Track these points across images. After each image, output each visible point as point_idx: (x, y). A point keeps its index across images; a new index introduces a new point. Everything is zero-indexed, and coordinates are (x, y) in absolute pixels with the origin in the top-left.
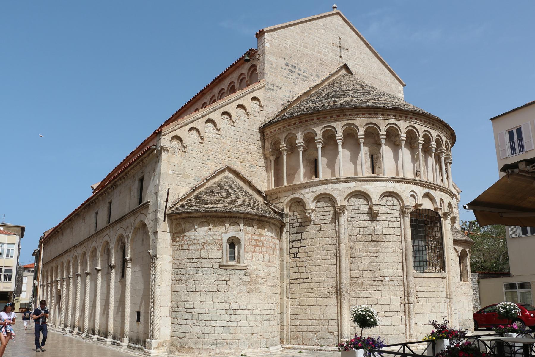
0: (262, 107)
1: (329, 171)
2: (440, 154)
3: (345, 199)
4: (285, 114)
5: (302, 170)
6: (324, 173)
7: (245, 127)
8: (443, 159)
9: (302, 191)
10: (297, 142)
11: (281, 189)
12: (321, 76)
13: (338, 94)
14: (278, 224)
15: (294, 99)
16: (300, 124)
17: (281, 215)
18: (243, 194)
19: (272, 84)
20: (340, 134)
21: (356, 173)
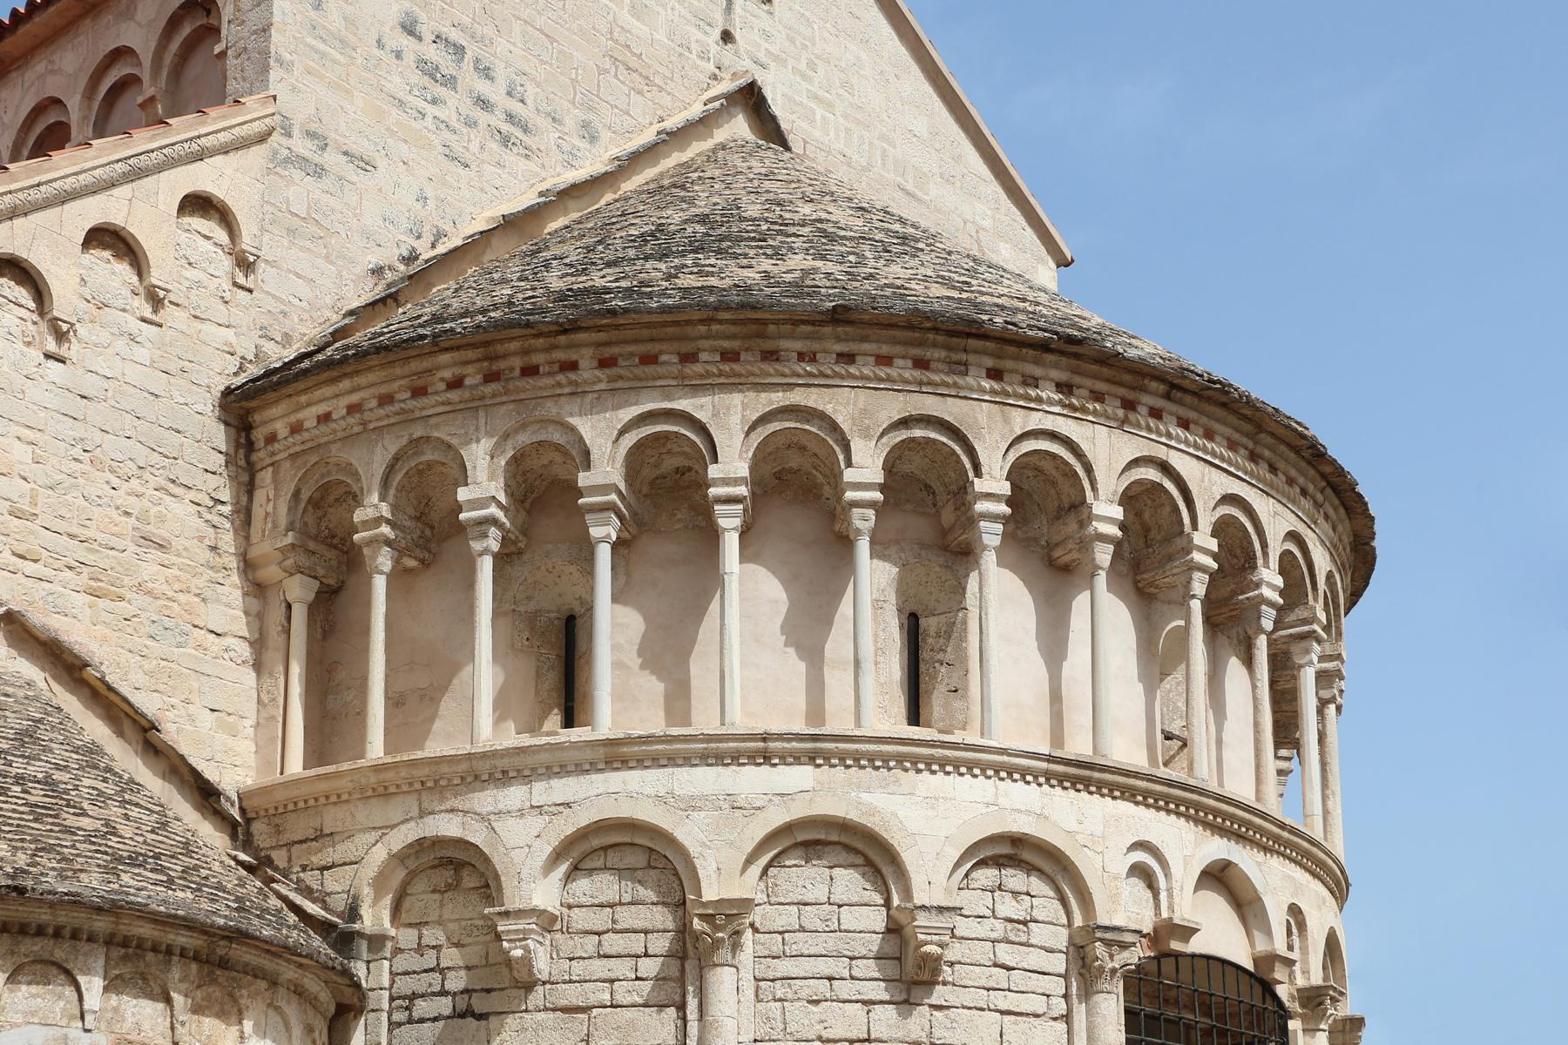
0: (245, 264)
1: (654, 687)
2: (1295, 648)
3: (749, 861)
4: (398, 321)
5: (485, 673)
6: (620, 697)
7: (134, 374)
8: (1308, 678)
9: (485, 800)
10: (463, 494)
11: (345, 784)
12: (605, 135)
13: (719, 235)
14: (325, 996)
15: (441, 249)
16: (489, 389)
17: (344, 940)
18: (110, 789)
19: (311, 135)
20: (732, 466)
21: (816, 710)
